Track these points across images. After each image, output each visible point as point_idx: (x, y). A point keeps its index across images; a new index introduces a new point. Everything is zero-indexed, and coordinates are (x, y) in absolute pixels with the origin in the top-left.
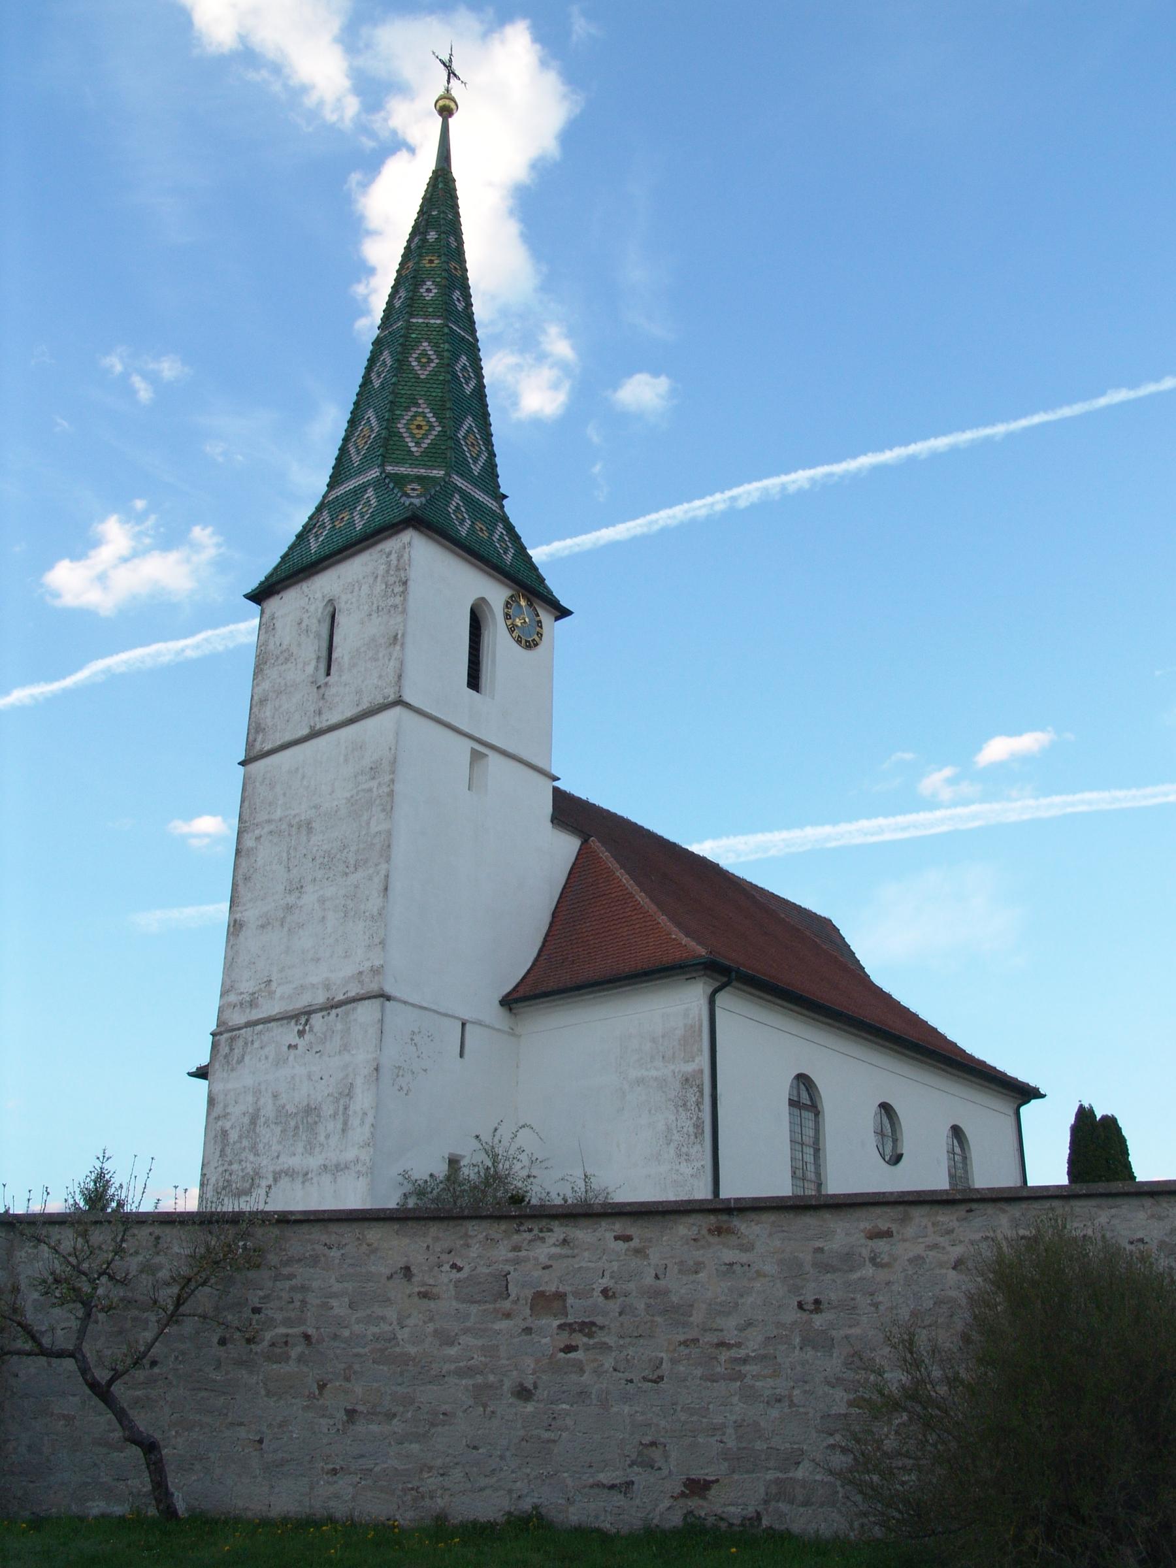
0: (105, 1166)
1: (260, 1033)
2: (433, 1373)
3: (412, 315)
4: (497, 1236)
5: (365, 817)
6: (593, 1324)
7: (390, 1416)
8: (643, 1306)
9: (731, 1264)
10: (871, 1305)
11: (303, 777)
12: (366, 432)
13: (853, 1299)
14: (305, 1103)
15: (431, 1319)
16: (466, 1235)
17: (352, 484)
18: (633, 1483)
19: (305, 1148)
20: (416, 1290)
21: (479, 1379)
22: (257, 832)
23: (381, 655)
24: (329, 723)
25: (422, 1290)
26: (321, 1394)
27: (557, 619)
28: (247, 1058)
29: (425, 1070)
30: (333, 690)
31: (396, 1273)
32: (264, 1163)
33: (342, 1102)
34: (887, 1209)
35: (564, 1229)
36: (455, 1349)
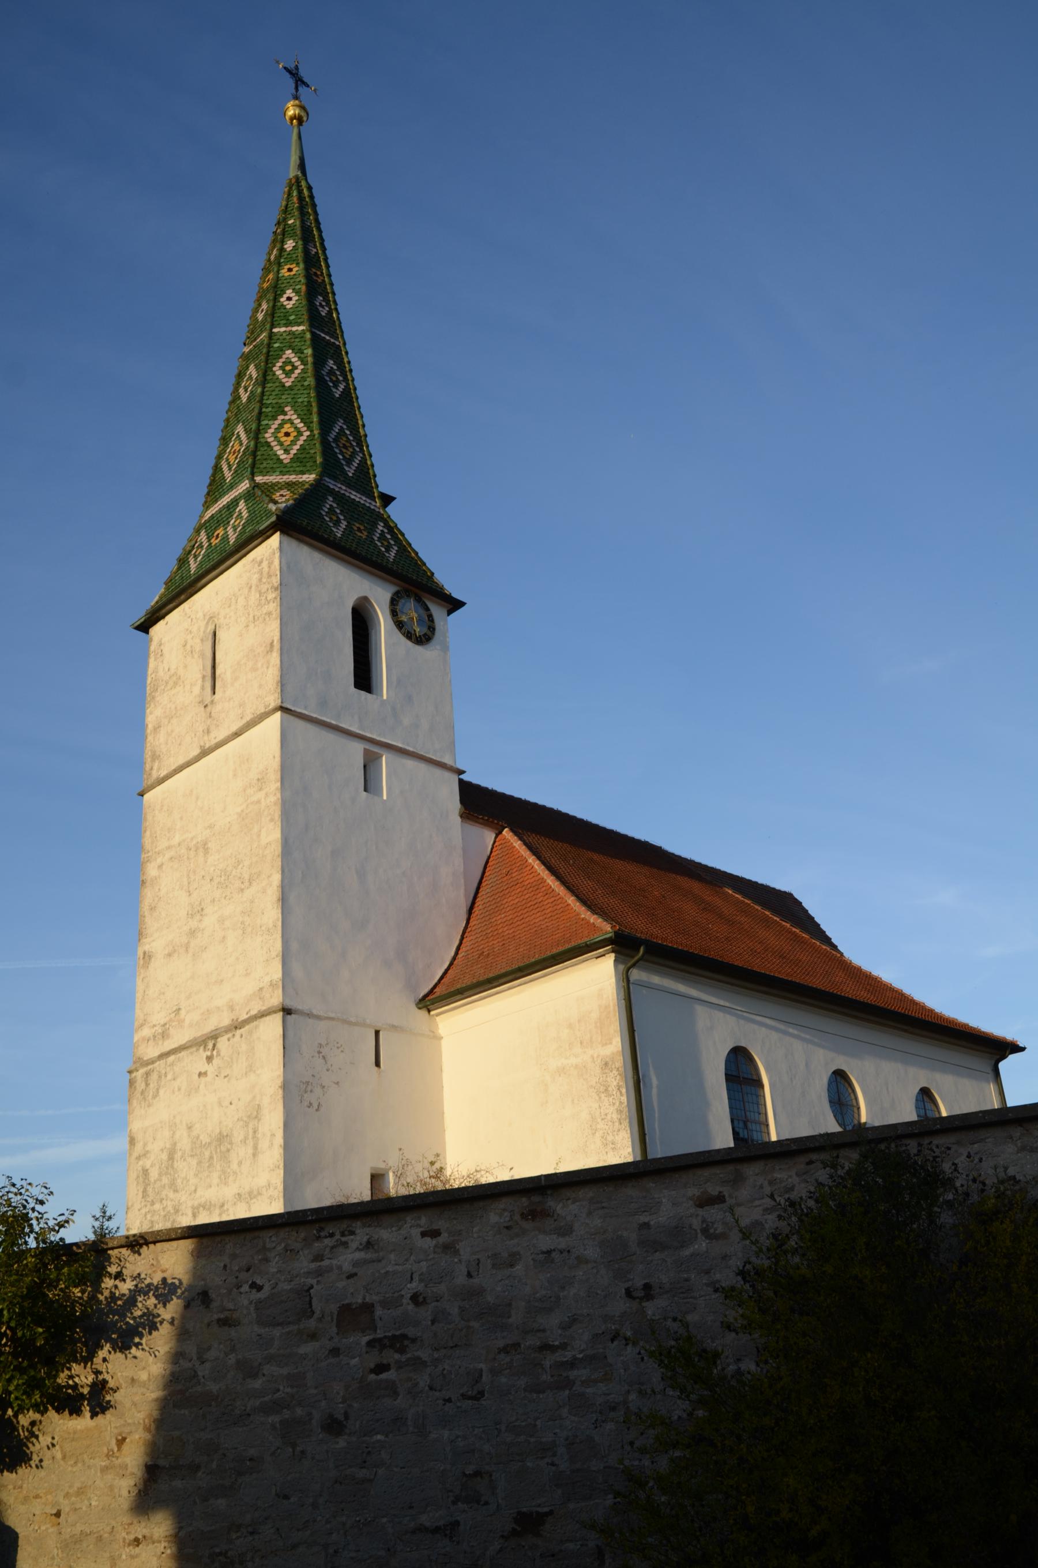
0: (106, 1224)
1: (172, 1064)
3: (273, 326)
5: (256, 830)
6: (404, 1336)
7: (194, 1468)
8: (456, 1310)
9: (549, 1252)
10: (707, 1285)
11: (197, 798)
12: (237, 447)
13: (687, 1280)
14: (218, 1131)
15: (233, 1349)
17: (225, 500)
18: (457, 1523)
19: (220, 1178)
20: (216, 1317)
21: (286, 1414)
22: (159, 860)
23: (259, 665)
24: (217, 740)
25: (222, 1316)
26: (119, 1449)
27: (450, 612)
28: (161, 1092)
29: (337, 1083)
30: (218, 707)
31: (193, 1300)
32: (183, 1199)
33: (251, 1125)
34: (717, 1170)
35: (367, 1230)
36: (260, 1382)
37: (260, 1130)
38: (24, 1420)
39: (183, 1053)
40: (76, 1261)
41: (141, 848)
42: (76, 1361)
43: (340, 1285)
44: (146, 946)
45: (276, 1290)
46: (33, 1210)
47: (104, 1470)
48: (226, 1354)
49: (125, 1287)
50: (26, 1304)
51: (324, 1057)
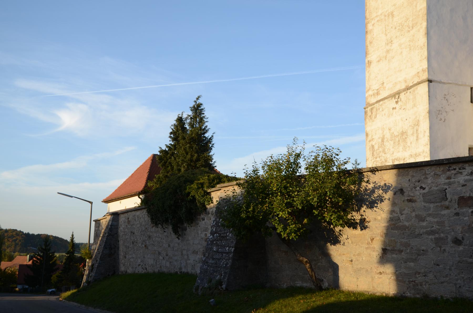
1: (382, 105)
2: (417, 233)
4: (439, 173)
14: (401, 131)
15: (414, 211)
16: (425, 174)
20: (406, 198)
21: (437, 236)
22: (373, 22)
25: (409, 198)
26: (372, 242)
28: (378, 116)
29: (453, 110)
31: (397, 192)
33: (415, 128)
36: (425, 223)
37: (419, 130)
38: (337, 229)
39: (386, 100)
40: (352, 176)
41: (365, 18)
42: (354, 211)
43: (459, 189)
44: (369, 58)
45: (431, 190)
46: (335, 157)
47: (367, 248)
48: (411, 212)
49: (370, 186)
50: (335, 190)
51: (447, 100)
